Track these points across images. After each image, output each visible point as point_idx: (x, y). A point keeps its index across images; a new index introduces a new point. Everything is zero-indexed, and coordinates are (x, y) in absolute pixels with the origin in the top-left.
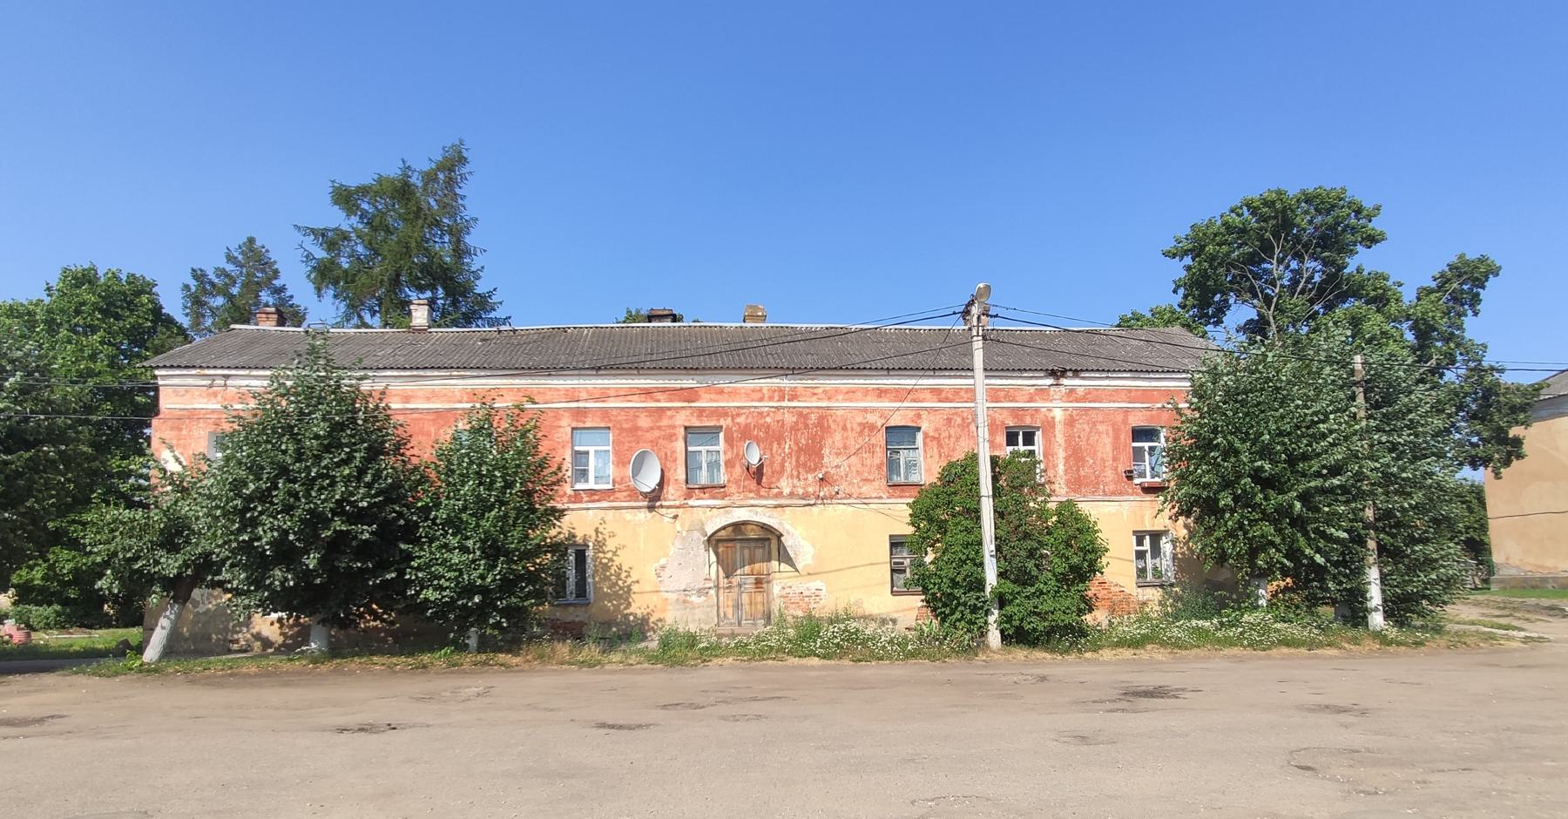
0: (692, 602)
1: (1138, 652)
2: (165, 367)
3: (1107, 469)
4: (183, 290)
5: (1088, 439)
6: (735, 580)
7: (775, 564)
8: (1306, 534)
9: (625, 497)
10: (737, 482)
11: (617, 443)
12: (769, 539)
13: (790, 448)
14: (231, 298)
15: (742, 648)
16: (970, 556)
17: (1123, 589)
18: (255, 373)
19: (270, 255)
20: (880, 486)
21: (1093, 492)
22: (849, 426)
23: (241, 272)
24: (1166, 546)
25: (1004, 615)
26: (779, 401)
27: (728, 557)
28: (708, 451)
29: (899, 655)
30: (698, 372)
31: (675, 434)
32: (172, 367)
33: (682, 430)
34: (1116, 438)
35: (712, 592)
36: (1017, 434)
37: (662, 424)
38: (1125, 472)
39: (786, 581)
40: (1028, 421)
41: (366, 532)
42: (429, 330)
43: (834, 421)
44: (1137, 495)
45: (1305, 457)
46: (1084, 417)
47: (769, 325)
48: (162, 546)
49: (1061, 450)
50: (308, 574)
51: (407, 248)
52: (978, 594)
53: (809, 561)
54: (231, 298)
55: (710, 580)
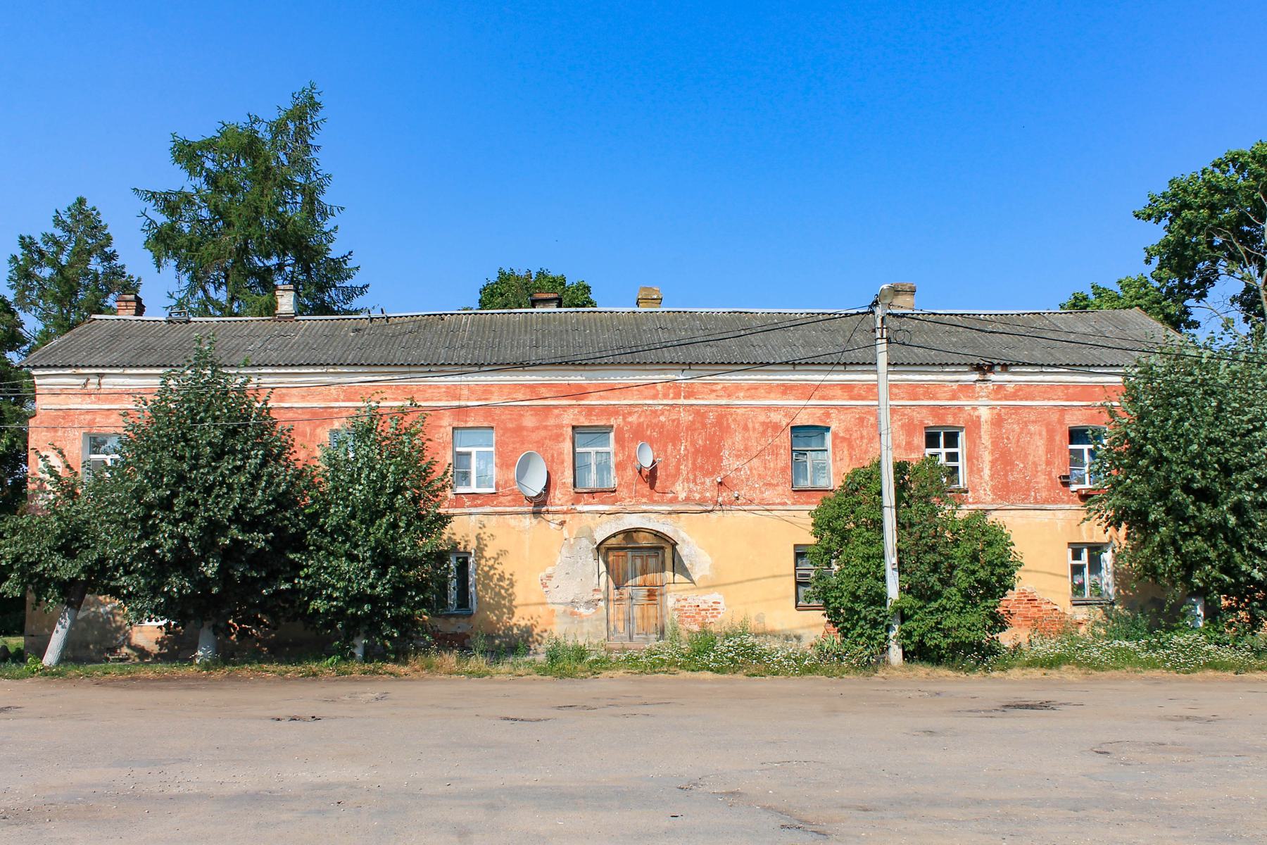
0: (580, 614)
1: (1049, 672)
2: (42, 366)
3: (1039, 474)
4: (10, 262)
5: (1018, 441)
6: (627, 591)
7: (669, 574)
8: (1240, 550)
9: (509, 502)
10: (628, 486)
11: (499, 444)
12: (662, 548)
13: (686, 449)
14: (61, 270)
15: (632, 662)
16: (871, 570)
17: (1055, 607)
18: (128, 371)
19: (100, 218)
20: (784, 491)
21: (1023, 500)
22: (750, 425)
23: (70, 238)
24: (1107, 557)
25: (904, 631)
26: (673, 398)
27: (618, 565)
28: (597, 453)
29: (795, 670)
30: (587, 368)
31: (562, 434)
32: (49, 366)
33: (570, 429)
34: (1051, 440)
35: (602, 604)
36: (938, 435)
37: (549, 424)
38: (1060, 477)
39: (681, 593)
40: (950, 421)
41: (259, 540)
42: (296, 318)
43: (734, 420)
44: (1074, 502)
45: (1241, 468)
46: (1013, 416)
47: (664, 309)
48: (59, 550)
49: (987, 453)
50: (205, 582)
51: (257, 212)
52: (879, 609)
53: (707, 572)
54: (61, 270)
55: (600, 591)
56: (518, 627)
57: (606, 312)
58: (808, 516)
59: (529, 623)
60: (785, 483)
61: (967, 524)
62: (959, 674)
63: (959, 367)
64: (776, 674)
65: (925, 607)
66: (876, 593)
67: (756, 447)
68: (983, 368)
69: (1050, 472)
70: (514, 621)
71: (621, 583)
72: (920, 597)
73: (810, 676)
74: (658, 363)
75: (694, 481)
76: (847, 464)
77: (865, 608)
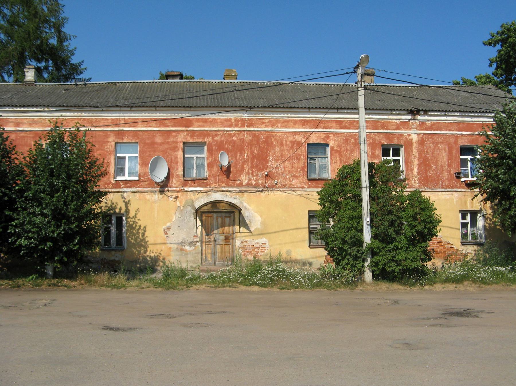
0: (186, 250)
1: (458, 286)
3: (444, 172)
5: (433, 153)
6: (213, 237)
7: (237, 227)
9: (146, 185)
10: (215, 176)
11: (141, 152)
12: (233, 212)
20: (303, 180)
21: (435, 186)
22: (284, 142)
26: (241, 127)
27: (208, 222)
28: (197, 157)
29: (308, 286)
30: (192, 109)
31: (177, 147)
33: (182, 144)
34: (450, 153)
35: (198, 244)
36: (389, 149)
37: (169, 141)
38: (455, 174)
39: (244, 238)
40: (396, 141)
43: (275, 140)
44: (463, 188)
46: (430, 139)
49: (416, 160)
52: (358, 249)
56: (150, 257)
57: (206, 82)
58: (317, 194)
59: (156, 255)
60: (304, 176)
61: (410, 198)
62: (406, 288)
63: (400, 111)
64: (297, 288)
65: (386, 247)
66: (357, 239)
67: (287, 154)
68: (414, 112)
69: (450, 171)
70: (148, 253)
71: (209, 232)
72: (382, 241)
73: (317, 289)
74: (232, 106)
75: (252, 174)
76: (339, 165)
77: (350, 248)
